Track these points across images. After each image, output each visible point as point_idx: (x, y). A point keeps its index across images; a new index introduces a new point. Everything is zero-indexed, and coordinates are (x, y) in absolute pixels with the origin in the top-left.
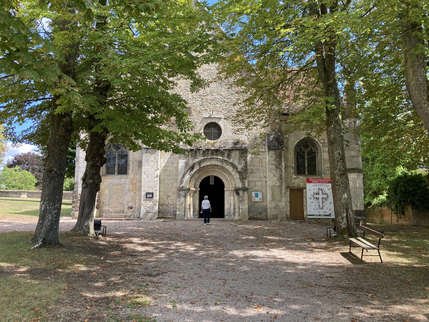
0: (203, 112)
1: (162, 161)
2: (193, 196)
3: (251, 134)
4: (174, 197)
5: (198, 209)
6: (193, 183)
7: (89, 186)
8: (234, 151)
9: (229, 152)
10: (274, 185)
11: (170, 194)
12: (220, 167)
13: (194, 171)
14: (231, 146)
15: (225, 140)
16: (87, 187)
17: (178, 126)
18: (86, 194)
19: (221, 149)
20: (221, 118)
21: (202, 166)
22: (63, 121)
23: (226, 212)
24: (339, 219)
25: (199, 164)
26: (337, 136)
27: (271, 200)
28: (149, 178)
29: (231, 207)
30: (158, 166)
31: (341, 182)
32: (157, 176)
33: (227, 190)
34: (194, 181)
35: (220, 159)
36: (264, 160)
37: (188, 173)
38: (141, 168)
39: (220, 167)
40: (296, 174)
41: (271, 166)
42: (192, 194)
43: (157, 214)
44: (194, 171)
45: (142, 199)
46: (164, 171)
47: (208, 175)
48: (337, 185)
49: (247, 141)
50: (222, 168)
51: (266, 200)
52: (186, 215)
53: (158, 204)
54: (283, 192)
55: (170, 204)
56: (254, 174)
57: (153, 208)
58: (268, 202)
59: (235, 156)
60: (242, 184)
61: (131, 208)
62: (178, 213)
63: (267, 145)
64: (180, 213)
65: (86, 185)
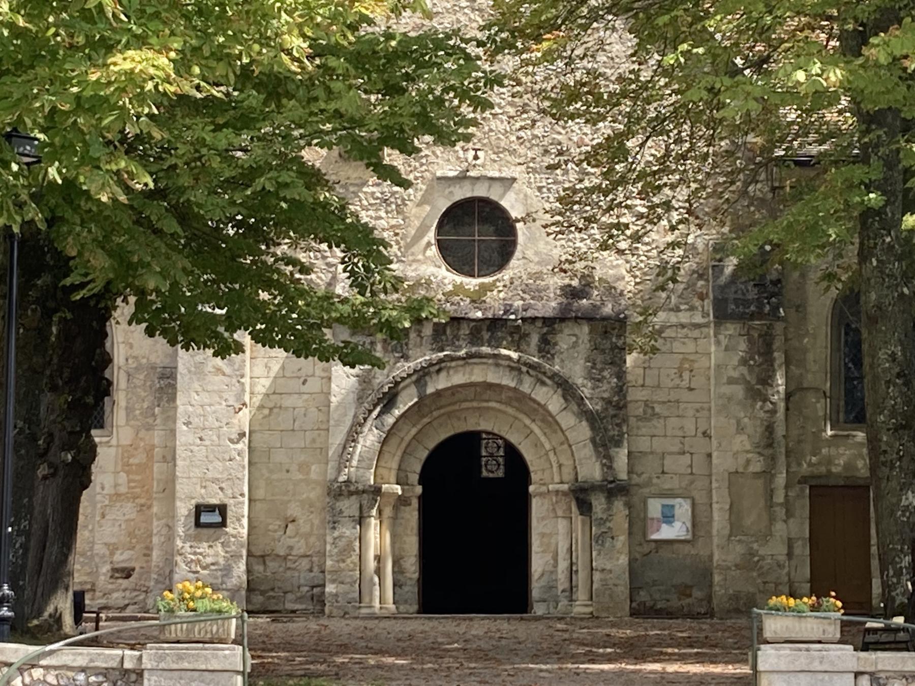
0: (434, 153)
1: (259, 370)
2: (395, 518)
3: (645, 248)
4: (312, 524)
5: (416, 575)
6: (395, 465)
7: (61, 473)
8: (570, 324)
9: (545, 330)
10: (741, 470)
11: (294, 510)
12: (511, 394)
13: (397, 412)
14: (553, 304)
15: (530, 276)
16: (53, 475)
17: (349, 278)
18: (50, 499)
19: (513, 317)
20: (514, 180)
21: (430, 390)
22: (35, 285)
23: (536, 589)
24: (887, 575)
25: (417, 382)
26: (887, 296)
27: (727, 532)
28: (207, 443)
29: (556, 565)
30: (243, 391)
31: (898, 453)
32: (242, 435)
33: (541, 495)
34: (399, 453)
35: (509, 358)
36: (702, 362)
37: (369, 422)
38: (173, 398)
39: (511, 394)
40: (842, 416)
41: (727, 390)
42: (388, 512)
43: (243, 593)
44: (397, 412)
45: (180, 531)
46: (266, 412)
47: (471, 428)
48: (884, 464)
49: (628, 278)
50: (518, 400)
51: (709, 534)
52: (366, 599)
53: (244, 552)
54: (780, 498)
55: (294, 553)
56: (655, 422)
57: (227, 570)
58: (716, 541)
59: (575, 345)
60: (603, 465)
61: (127, 573)
62: (330, 588)
63: (711, 296)
64: (342, 588)
65: (49, 468)
